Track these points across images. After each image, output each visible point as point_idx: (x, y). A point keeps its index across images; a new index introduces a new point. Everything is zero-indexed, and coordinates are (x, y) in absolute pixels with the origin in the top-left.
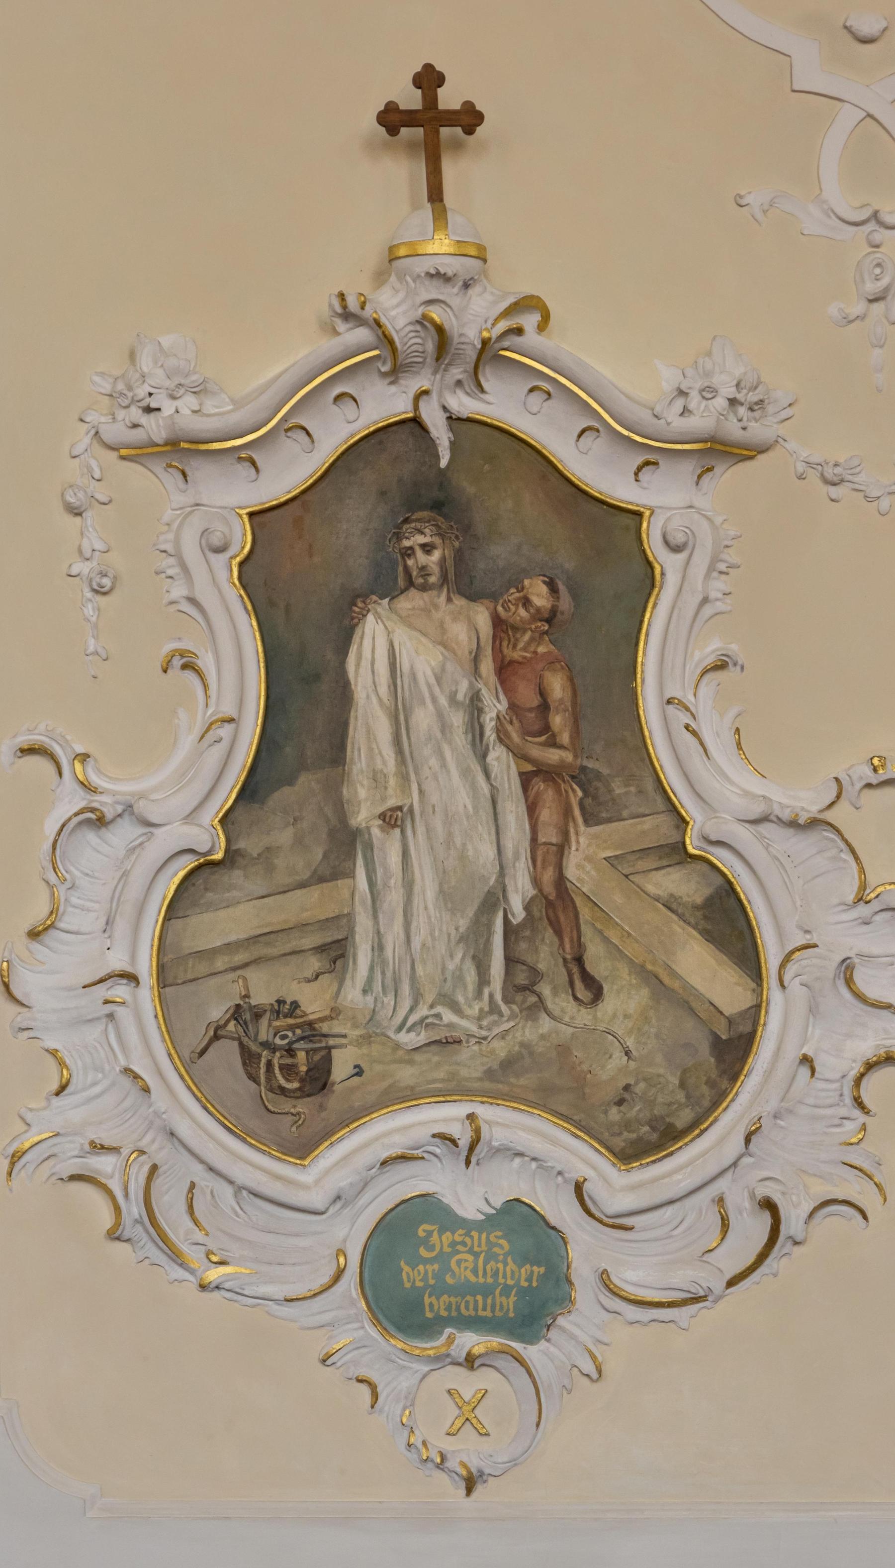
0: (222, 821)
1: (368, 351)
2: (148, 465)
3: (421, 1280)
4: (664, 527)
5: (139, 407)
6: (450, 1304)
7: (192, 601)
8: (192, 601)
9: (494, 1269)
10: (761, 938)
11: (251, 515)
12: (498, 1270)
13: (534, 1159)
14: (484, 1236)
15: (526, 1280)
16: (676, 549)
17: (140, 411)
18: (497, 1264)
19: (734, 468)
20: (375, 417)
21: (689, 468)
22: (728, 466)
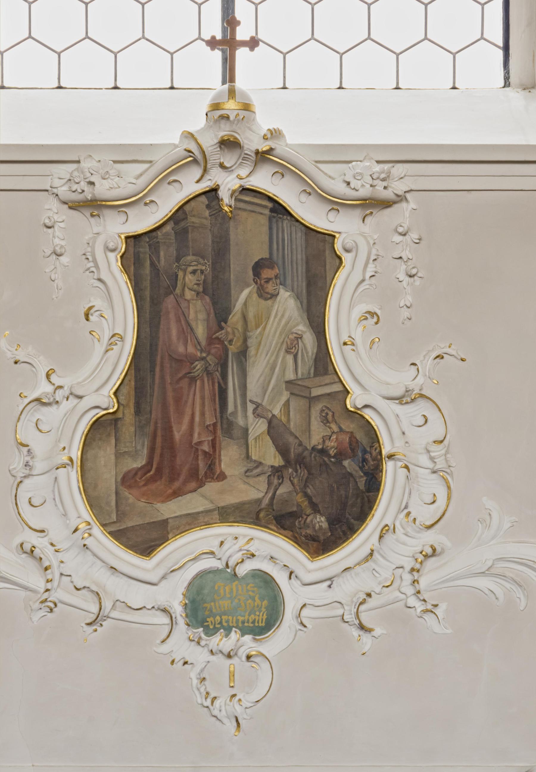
0: (115, 393)
1: (286, 162)
2: (82, 212)
3: (219, 624)
4: (343, 242)
5: (86, 182)
7: (100, 280)
8: (100, 280)
9: (253, 619)
10: (353, 540)
11: (127, 238)
12: (255, 619)
14: (223, 610)
16: (347, 251)
17: (86, 183)
18: (255, 616)
19: (379, 213)
20: (255, 184)
21: (358, 213)
22: (377, 211)
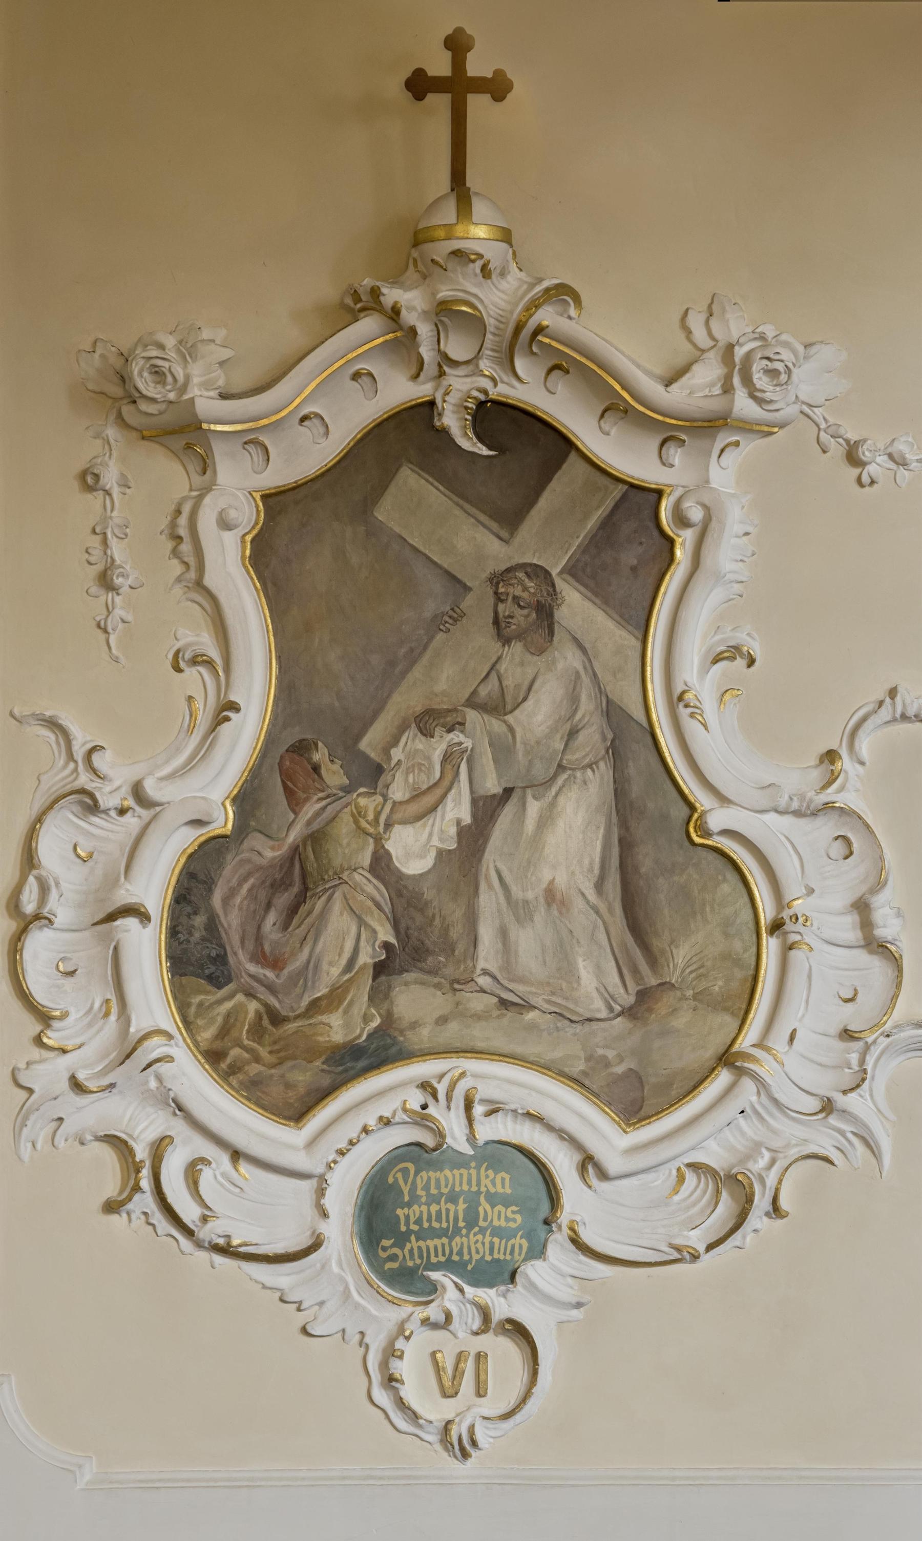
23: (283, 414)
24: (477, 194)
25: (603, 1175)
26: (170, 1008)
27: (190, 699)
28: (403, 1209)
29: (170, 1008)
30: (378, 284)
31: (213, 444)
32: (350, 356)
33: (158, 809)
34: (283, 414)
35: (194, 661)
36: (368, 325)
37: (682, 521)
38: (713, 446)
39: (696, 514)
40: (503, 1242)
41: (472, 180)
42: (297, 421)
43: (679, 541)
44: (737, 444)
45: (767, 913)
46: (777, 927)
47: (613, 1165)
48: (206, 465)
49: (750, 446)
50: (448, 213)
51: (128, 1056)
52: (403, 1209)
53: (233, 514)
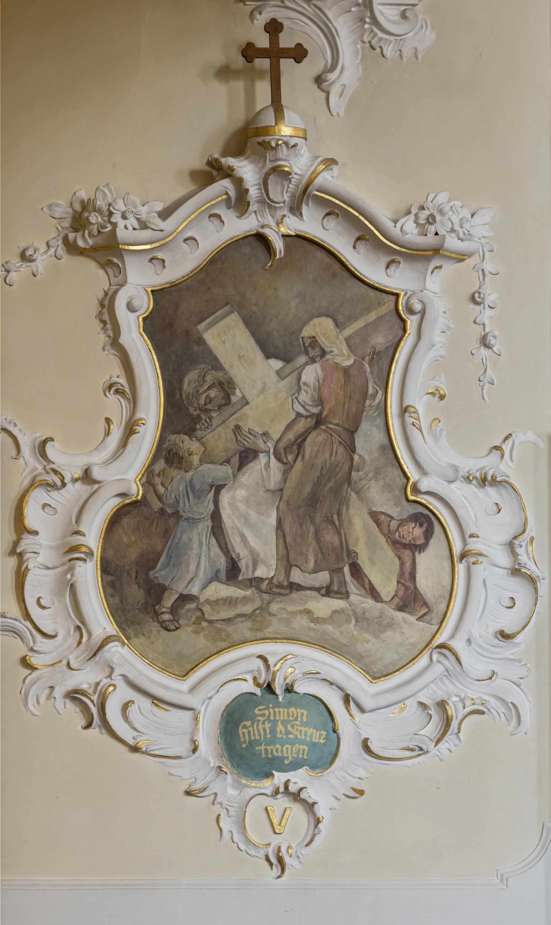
6: (299, 749)
13: (436, 679)
15: (302, 755)
23: (168, 240)
24: (287, 107)
25: (362, 710)
26: (109, 618)
27: (108, 421)
28: (270, 746)
29: (109, 618)
30: (106, 306)
31: (125, 257)
32: (213, 202)
33: (96, 486)
34: (168, 240)
35: (117, 392)
36: (226, 184)
37: (411, 311)
38: (428, 266)
39: (418, 307)
40: (253, 738)
41: (284, 101)
42: (183, 240)
43: (409, 322)
44: (440, 267)
45: (457, 547)
46: (463, 556)
47: (367, 703)
48: (120, 270)
49: (449, 268)
50: (269, 119)
51: (95, 655)
52: (270, 746)
53: (136, 303)
